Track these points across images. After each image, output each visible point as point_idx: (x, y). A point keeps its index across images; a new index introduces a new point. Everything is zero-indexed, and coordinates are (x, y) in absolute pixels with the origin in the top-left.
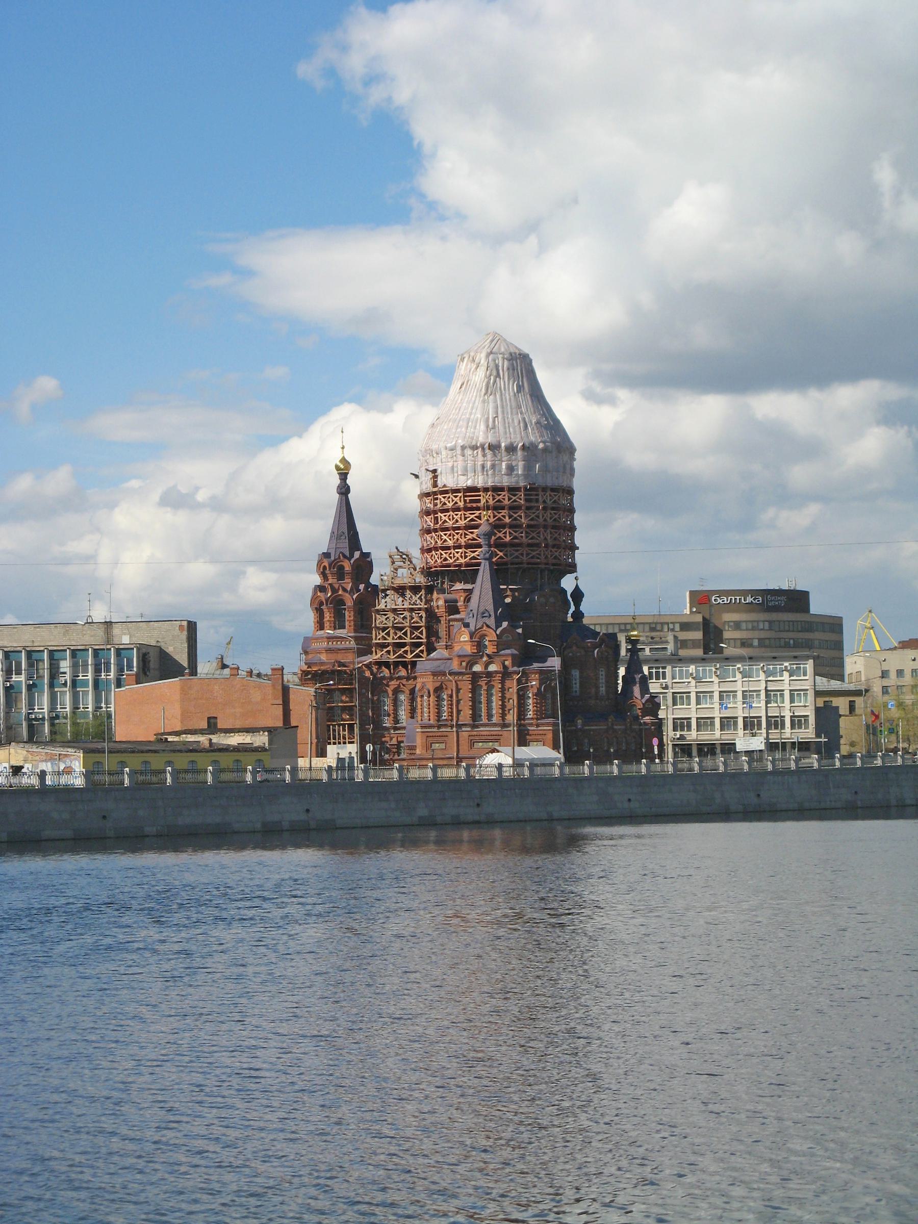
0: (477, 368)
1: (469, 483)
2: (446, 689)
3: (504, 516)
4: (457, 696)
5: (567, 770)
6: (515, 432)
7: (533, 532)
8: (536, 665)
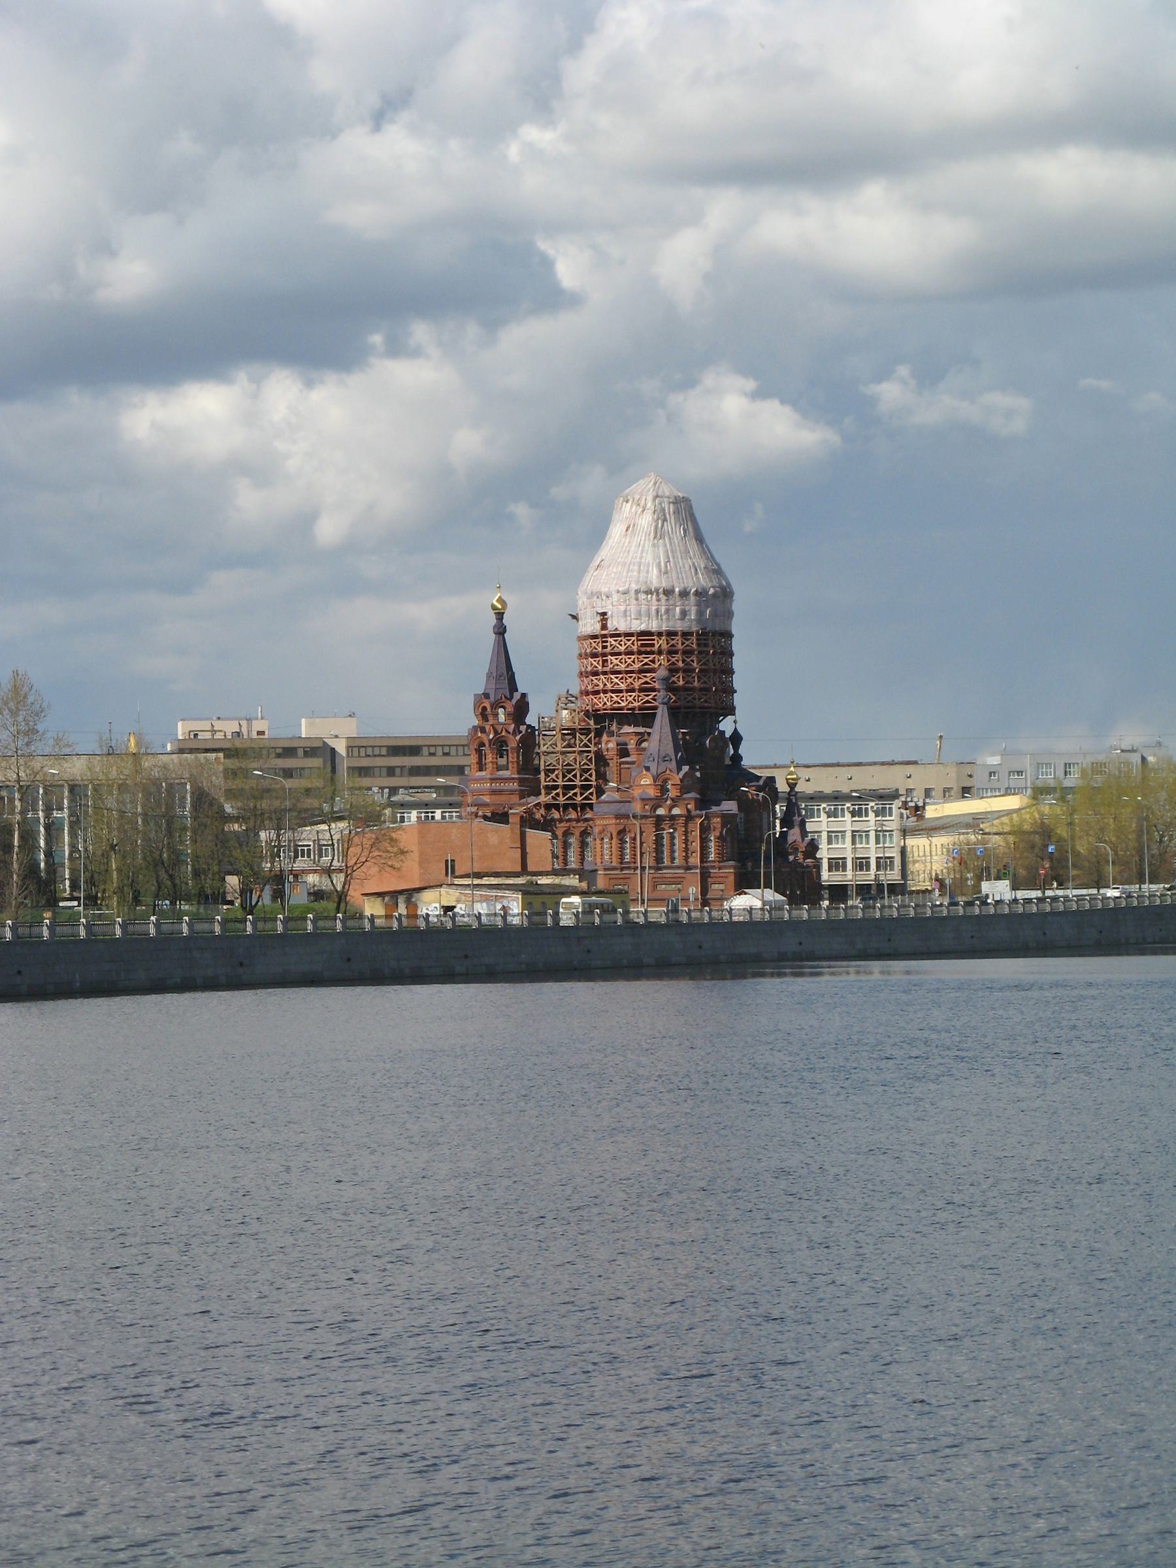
0: (643, 511)
1: (643, 627)
6: (687, 578)
8: (714, 809)
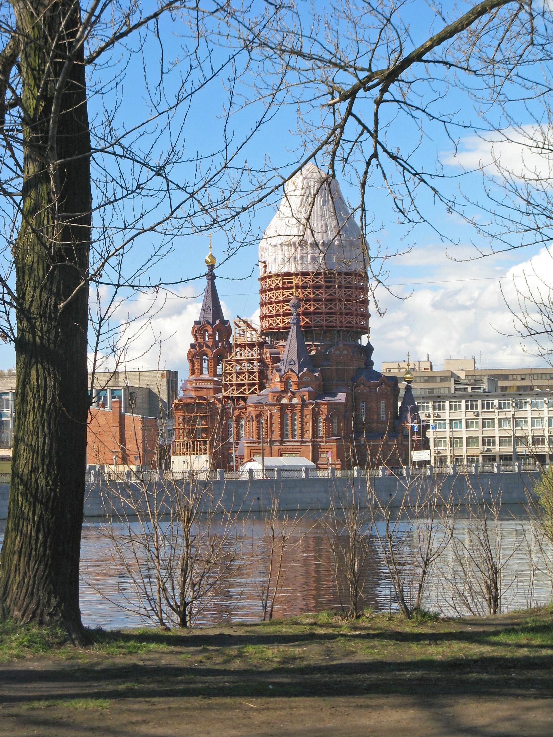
2: (322, 414)
3: (310, 293)
4: (271, 421)
5: (503, 468)
7: (331, 304)
8: (327, 398)
